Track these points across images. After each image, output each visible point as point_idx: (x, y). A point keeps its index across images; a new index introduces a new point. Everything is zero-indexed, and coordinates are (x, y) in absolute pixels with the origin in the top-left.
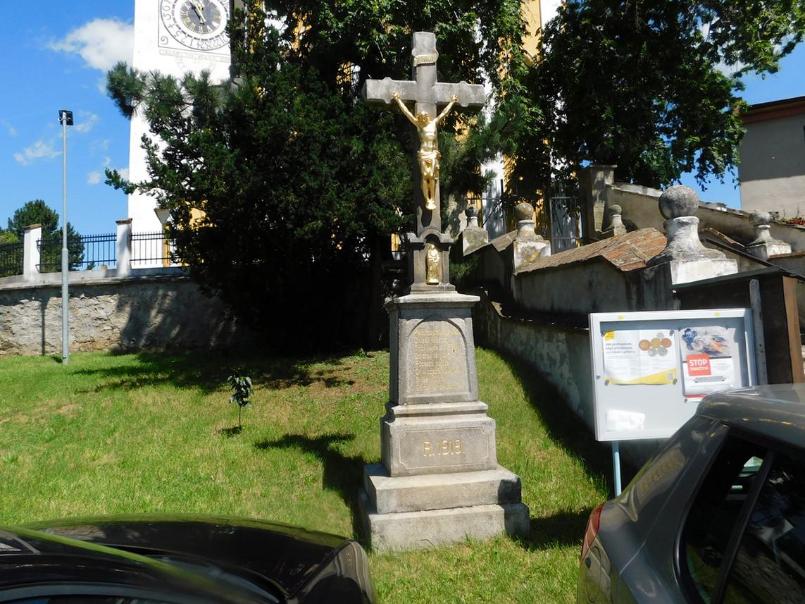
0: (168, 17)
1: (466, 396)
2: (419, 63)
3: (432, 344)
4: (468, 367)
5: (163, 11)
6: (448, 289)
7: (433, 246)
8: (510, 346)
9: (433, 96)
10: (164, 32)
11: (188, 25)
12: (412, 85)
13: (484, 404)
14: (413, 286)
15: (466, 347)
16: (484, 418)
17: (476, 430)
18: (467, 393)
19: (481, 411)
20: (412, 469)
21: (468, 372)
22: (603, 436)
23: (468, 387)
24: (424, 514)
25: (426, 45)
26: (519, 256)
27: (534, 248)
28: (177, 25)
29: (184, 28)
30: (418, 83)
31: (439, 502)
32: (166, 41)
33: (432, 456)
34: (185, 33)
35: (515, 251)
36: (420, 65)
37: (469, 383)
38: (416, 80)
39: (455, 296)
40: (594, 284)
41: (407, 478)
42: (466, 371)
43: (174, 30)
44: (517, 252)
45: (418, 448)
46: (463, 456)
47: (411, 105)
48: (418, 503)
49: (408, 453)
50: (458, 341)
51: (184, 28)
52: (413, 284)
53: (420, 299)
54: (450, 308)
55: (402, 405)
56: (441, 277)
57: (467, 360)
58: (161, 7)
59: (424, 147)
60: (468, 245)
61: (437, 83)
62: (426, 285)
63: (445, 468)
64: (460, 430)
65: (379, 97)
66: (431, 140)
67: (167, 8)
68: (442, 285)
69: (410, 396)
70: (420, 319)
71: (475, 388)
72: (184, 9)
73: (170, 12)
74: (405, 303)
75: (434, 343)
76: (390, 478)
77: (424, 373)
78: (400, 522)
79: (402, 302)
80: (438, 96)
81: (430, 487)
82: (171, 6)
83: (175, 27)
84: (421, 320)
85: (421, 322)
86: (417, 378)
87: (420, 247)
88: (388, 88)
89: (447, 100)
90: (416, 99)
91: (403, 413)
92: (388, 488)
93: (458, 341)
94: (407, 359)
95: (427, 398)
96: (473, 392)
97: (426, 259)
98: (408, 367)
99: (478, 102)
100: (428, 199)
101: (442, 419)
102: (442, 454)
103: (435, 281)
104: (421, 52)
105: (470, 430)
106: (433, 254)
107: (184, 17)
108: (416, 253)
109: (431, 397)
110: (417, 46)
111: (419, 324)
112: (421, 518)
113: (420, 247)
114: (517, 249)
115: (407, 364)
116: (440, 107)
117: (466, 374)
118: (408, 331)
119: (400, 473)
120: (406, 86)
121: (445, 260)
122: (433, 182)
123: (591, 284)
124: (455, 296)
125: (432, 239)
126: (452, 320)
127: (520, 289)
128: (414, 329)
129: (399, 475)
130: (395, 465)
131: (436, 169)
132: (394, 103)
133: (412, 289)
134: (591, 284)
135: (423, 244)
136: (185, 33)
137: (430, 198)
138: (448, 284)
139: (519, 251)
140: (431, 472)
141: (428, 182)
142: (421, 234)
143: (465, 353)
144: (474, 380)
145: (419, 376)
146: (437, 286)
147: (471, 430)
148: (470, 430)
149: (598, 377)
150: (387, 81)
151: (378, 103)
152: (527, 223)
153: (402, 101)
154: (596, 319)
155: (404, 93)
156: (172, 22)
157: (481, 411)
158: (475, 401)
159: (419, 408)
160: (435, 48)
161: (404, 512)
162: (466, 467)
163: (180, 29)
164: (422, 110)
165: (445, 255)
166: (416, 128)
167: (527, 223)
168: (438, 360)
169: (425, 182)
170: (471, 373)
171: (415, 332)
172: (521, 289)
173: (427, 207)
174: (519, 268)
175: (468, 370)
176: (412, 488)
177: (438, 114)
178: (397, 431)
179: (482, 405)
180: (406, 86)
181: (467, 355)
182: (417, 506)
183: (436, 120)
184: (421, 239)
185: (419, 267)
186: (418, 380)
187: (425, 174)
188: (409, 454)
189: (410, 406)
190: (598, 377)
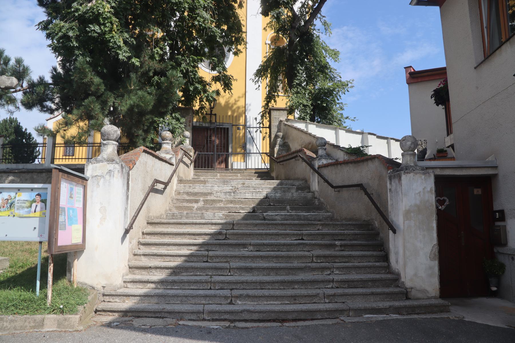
167: (165, 143)
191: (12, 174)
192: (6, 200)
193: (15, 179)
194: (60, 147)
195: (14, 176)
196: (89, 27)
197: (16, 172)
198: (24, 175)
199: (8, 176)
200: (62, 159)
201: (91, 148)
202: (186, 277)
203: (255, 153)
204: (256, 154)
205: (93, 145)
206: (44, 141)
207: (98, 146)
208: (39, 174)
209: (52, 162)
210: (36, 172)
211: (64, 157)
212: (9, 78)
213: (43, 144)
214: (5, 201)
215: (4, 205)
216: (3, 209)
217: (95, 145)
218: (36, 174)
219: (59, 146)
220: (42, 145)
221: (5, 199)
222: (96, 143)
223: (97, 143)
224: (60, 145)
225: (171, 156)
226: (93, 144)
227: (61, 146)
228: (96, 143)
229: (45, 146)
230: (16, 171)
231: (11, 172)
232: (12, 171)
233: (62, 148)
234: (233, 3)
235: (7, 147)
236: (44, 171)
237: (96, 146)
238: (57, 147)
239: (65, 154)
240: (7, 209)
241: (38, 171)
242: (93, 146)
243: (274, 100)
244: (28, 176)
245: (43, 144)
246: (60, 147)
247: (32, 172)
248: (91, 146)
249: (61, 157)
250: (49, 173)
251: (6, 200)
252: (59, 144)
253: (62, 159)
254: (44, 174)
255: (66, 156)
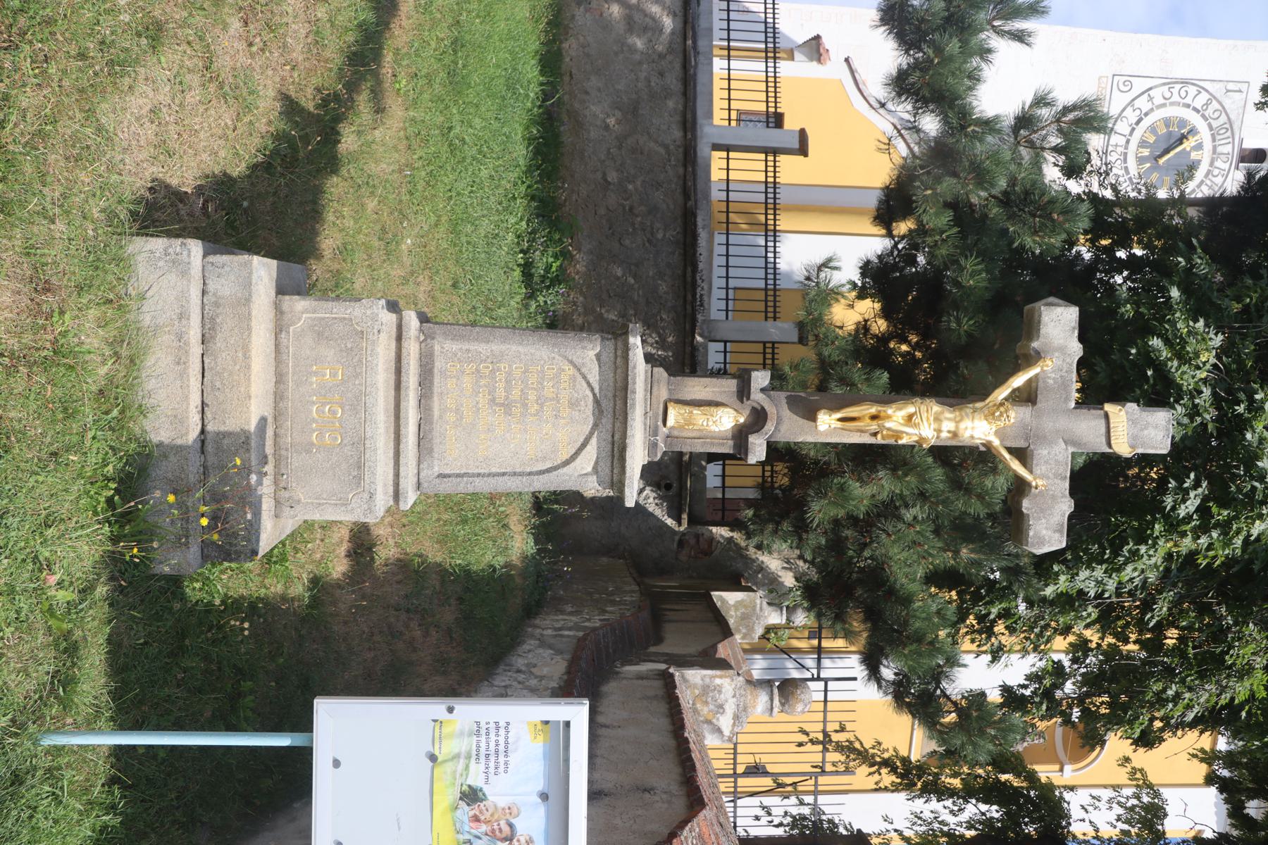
0: (1168, 95)
1: (431, 467)
2: (1111, 415)
3: (541, 401)
4: (489, 475)
5: (1178, 86)
6: (653, 446)
7: (742, 420)
8: (526, 647)
9: (1043, 439)
10: (1140, 86)
11: (1153, 129)
12: (1067, 399)
13: (410, 503)
14: (660, 372)
15: (530, 474)
16: (383, 500)
17: (359, 479)
18: (436, 470)
19: (397, 495)
20: (289, 340)
21: (479, 475)
22: (327, 711)
23: (447, 472)
24: (196, 350)
25: (1146, 432)
26: (707, 680)
27: (721, 707)
28: (1152, 110)
29: (1147, 122)
30: (1069, 410)
31: (218, 384)
32: (1122, 88)
33: (311, 384)
34: (1138, 123)
35: (718, 672)
36: (1107, 416)
37: (458, 476)
38: (1075, 408)
39: (637, 458)
40: (647, 795)
41: (271, 326)
42: (482, 471)
43: (1143, 104)
44: (717, 676)
45: (329, 353)
46: (308, 448)
47: (1027, 396)
48: (219, 343)
49: (321, 332)
50: (544, 459)
51: (1147, 122)
52: (665, 375)
53: (634, 379)
54: (613, 444)
55: (421, 330)
56: (676, 433)
57: (504, 474)
58: (1185, 82)
59: (942, 413)
60: (731, 602)
61: (1071, 449)
62: (662, 400)
63: (286, 408)
64: (361, 444)
65: (1043, 331)
66: (957, 427)
67: (1183, 94)
68: (660, 433)
69: (437, 348)
70: (601, 389)
71: (446, 487)
72: (1182, 123)
73: (1176, 98)
74: (627, 348)
75: (542, 405)
76: (273, 293)
77: (483, 382)
78: (183, 297)
79: (632, 340)
80: (1045, 452)
81: (248, 367)
82: (1188, 100)
83: (1149, 106)
84: (597, 391)
85: (592, 390)
86: (473, 366)
87: (743, 392)
88: (1062, 349)
89: (1037, 470)
90: (1039, 405)
91: (404, 328)
92: (254, 281)
93: (544, 459)
94: (514, 348)
95: (432, 382)
96: (437, 481)
97: (717, 404)
98: (496, 347)
99: (1031, 533)
100: (839, 415)
101: (386, 410)
102: (314, 403)
103: (671, 421)
104: (1132, 421)
105: (359, 467)
106: (726, 420)
107: (1167, 122)
108: (731, 385)
109: (432, 393)
110: (1145, 414)
111: (584, 377)
112: (187, 344)
113: (743, 392)
114: (721, 677)
115: (503, 347)
116: (1021, 454)
117: (476, 471)
118: (571, 354)
119: (282, 313)
120: (1065, 386)
121: (712, 444)
122: (874, 426)
123: (646, 790)
124: (637, 458)
125: (758, 419)
126: (594, 441)
127: (640, 677)
128: (575, 366)
129: (279, 311)
130: (298, 305)
131: (898, 435)
132: (1031, 359)
133: (656, 369)
134: (646, 790)
135: (748, 399)
136: (1138, 123)
137: (841, 420)
138: (662, 447)
139: (718, 681)
140: (280, 378)
141: (874, 417)
142: (769, 396)
143: (518, 470)
144: (464, 487)
145: (478, 371)
146: (660, 423)
147: (359, 469)
148: (359, 467)
149: (451, 710)
150: (1076, 349)
151: (1030, 328)
152: (772, 700)
153: (1037, 376)
154: (577, 713)
155: (1051, 382)
156: (1158, 100)
157: (397, 495)
158: (419, 485)
159: (412, 367)
160: (1140, 451)
161: (203, 309)
162: (283, 452)
163: (1146, 114)
164: (1015, 415)
165: (723, 444)
166: (984, 400)
167: (772, 700)
168: (508, 413)
169: (873, 410)
170: (477, 480)
171: (567, 367)
172: (642, 678)
173: (823, 411)
174: (685, 680)
175: (484, 475)
176: (249, 329)
177: (1010, 450)
178: (369, 312)
179: (410, 498)
180: (1065, 386)
181: (515, 474)
182: (213, 338)
183: (996, 442)
184: (757, 397)
185: (698, 388)
186: (470, 368)
187: (890, 411)
188: (320, 335)
189: (417, 346)
190: (451, 710)
191: (680, 26)
192: (506, 829)
193: (664, 36)
194: (767, 102)
195: (673, 33)
196: (1197, 485)
197: (685, 39)
198: (678, 66)
199: (675, 15)
200: (729, 109)
201: (762, 198)
202: (405, 344)
203: (735, 759)
204: (732, 761)
205: (769, 206)
206: (785, 51)
207: (766, 18)
208: (678, 118)
209: (717, 147)
210: (685, 107)
211: (734, 115)
212: (1060, 531)
213: (775, 183)
214: (503, 823)
215: (487, 822)
216: (466, 819)
217: (771, 212)
218: (680, 107)
219: (770, 99)
220: (771, 212)
221: (513, 821)
222: (775, 214)
223: (778, 217)
224: (773, 99)
225: (727, 732)
226: (775, 204)
227: (770, 84)
228: (775, 214)
229: (769, 55)
230: (689, 42)
231: (685, 22)
232: (689, 26)
233: (762, 177)
234: (1235, 833)
235: (766, 42)
236: (689, 136)
237: (766, 214)
238: (766, 161)
239: (743, 117)
240: (467, 837)
241: (689, 116)
242: (766, 203)
243: (900, 784)
244: (674, 81)
245: (775, 47)
246: (767, 102)
247: (685, 94)
248: (766, 198)
249: (734, 105)
250: (681, 150)
251: (511, 826)
252: (776, 92)
253: (729, 109)
254: (678, 134)
255: (738, 120)
